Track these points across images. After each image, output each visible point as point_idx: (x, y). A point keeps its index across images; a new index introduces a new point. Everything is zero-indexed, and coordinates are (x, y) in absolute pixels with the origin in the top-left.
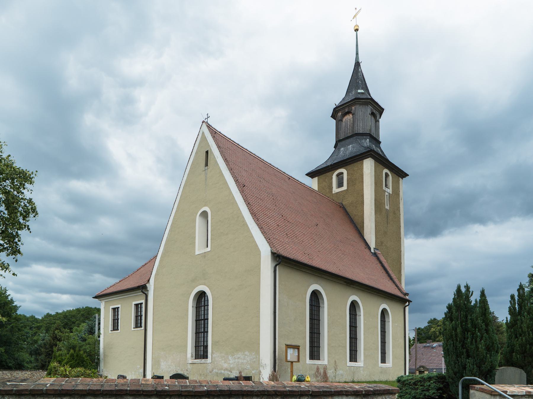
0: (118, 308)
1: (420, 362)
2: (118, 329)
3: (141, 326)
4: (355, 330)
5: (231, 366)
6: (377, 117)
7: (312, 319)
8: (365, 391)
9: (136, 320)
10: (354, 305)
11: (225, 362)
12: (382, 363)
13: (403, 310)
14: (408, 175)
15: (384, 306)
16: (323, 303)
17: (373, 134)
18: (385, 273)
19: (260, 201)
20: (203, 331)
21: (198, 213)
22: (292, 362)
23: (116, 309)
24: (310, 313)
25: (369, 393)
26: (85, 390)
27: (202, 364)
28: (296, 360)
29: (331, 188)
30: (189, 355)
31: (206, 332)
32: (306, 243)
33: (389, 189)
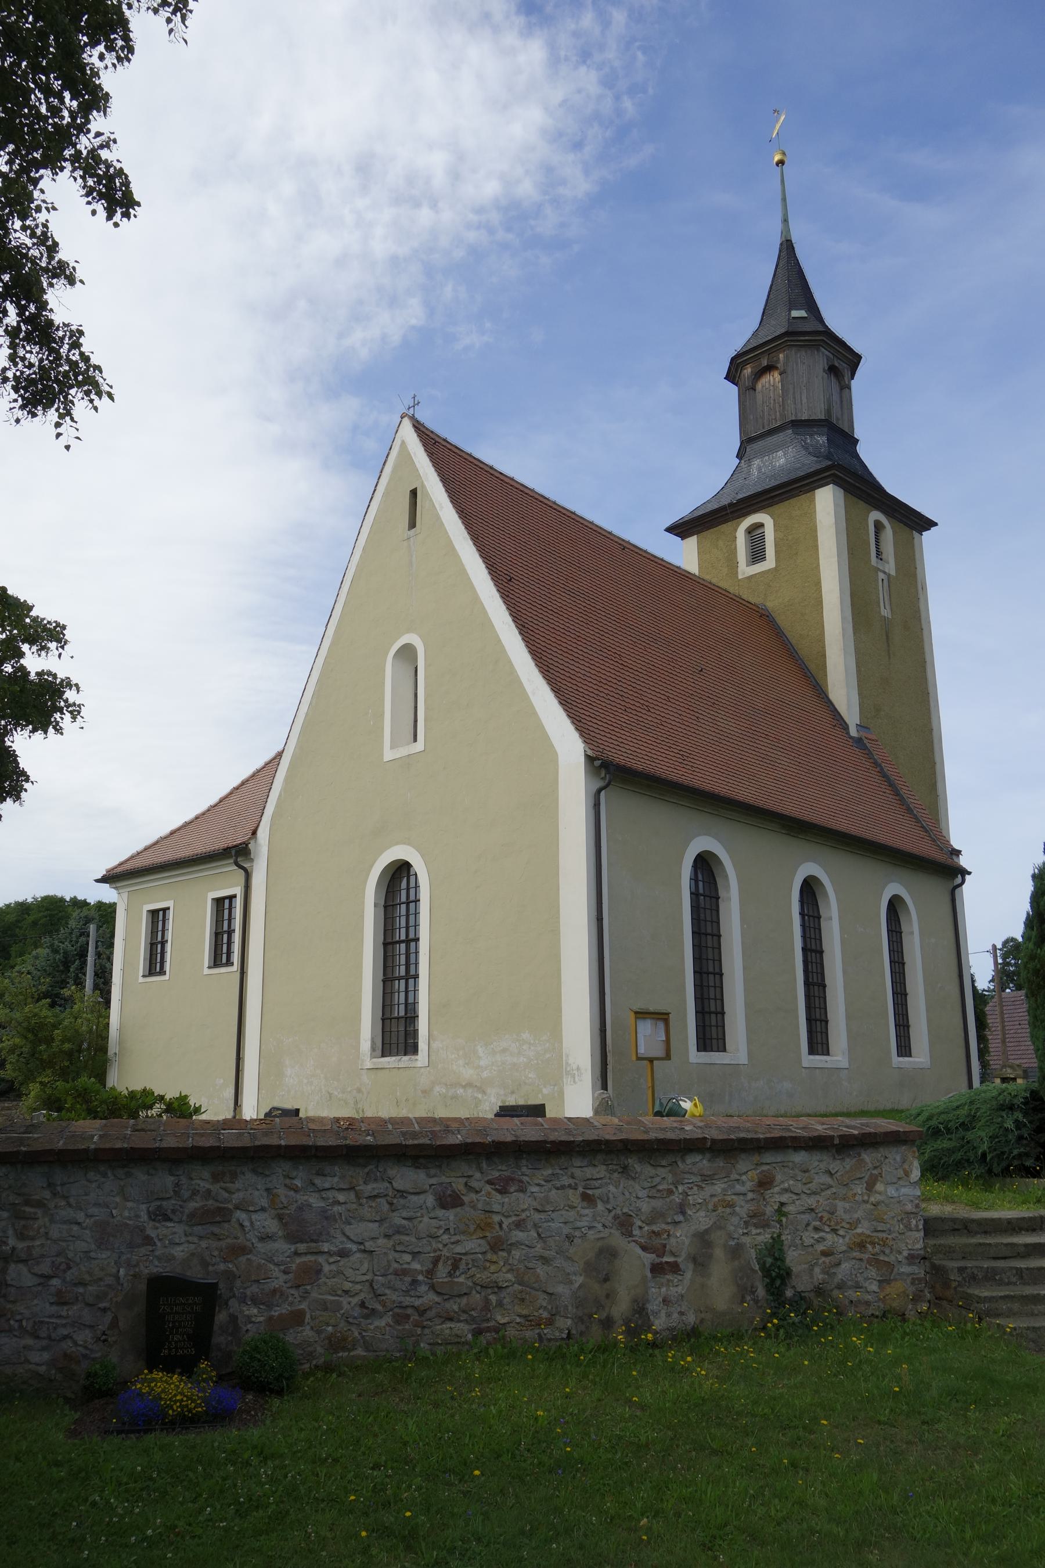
0: (165, 910)
1: (1017, 1048)
2: (162, 972)
3: (229, 963)
4: (818, 961)
5: (485, 1074)
6: (843, 376)
7: (699, 934)
8: (841, 1137)
9: (216, 945)
10: (811, 888)
11: (467, 1064)
12: (902, 1056)
13: (947, 899)
14: (936, 524)
15: (894, 888)
16: (727, 887)
17: (838, 419)
18: (892, 793)
19: (552, 617)
20: (403, 973)
21: (390, 648)
22: (651, 1060)
23: (161, 913)
24: (694, 917)
25: (851, 1143)
26: (185, 1149)
27: (401, 1070)
28: (660, 1052)
29: (733, 565)
30: (366, 1045)
31: (412, 976)
32: (673, 723)
33: (888, 563)
